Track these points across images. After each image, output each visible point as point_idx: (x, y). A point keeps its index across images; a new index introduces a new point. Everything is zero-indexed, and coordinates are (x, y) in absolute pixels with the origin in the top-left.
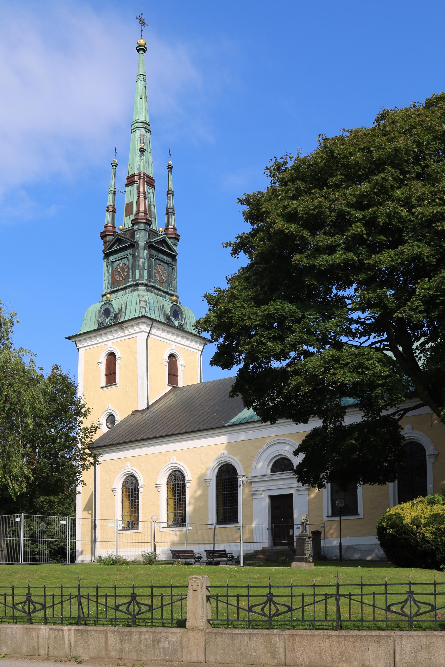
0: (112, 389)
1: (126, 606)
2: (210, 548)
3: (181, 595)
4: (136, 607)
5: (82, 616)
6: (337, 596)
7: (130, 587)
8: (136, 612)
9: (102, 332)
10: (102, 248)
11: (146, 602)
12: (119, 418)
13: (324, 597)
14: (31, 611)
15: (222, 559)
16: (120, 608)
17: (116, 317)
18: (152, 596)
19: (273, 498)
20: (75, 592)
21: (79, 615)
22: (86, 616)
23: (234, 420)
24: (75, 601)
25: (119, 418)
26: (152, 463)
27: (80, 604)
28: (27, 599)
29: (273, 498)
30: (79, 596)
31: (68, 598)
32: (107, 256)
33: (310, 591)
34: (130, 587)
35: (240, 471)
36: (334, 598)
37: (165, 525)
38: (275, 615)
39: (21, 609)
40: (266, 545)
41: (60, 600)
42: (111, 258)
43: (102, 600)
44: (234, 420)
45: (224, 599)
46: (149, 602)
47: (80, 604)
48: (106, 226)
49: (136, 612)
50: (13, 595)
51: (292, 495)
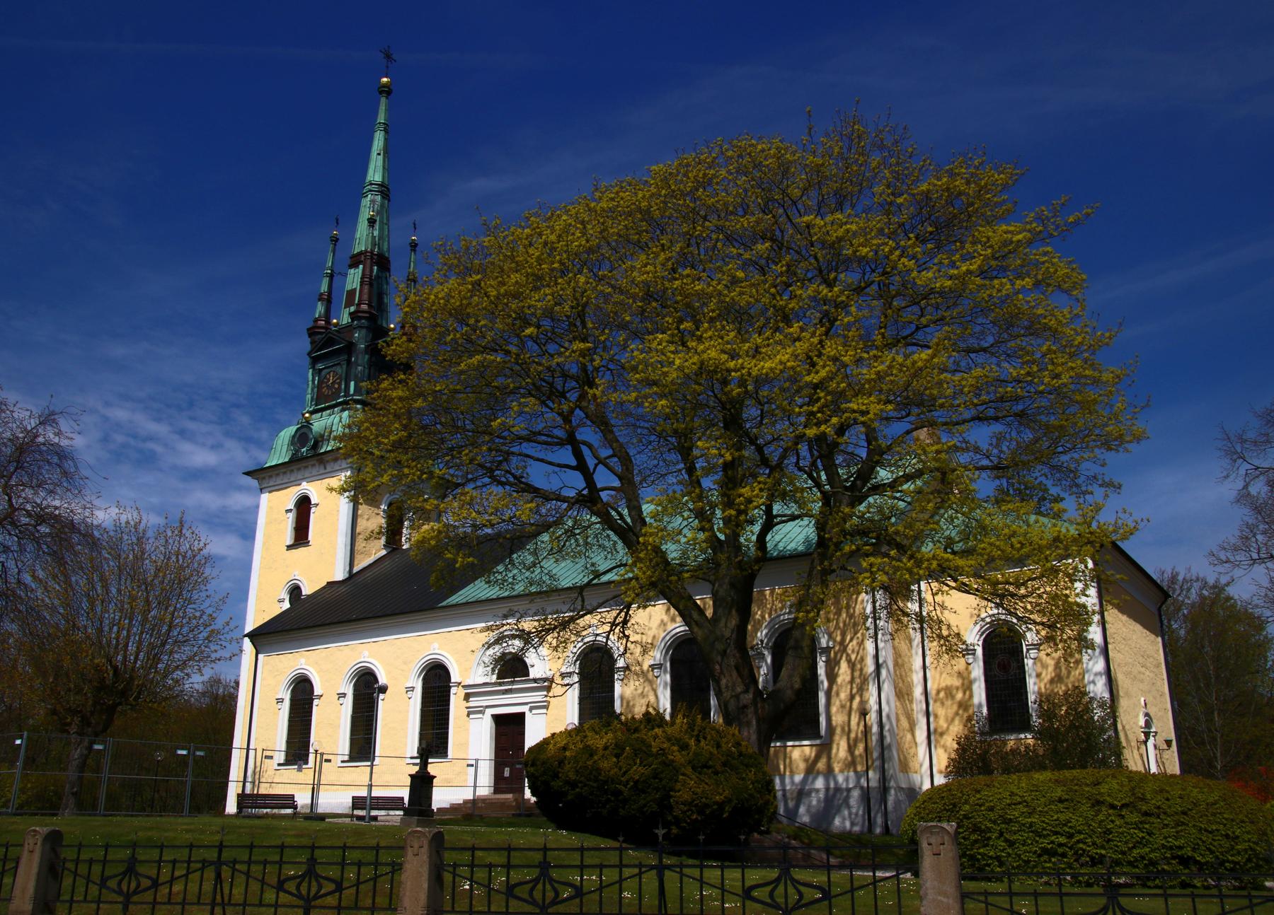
0: (302, 551)
1: (769, 888)
2: (363, 793)
3: (393, 864)
4: (791, 890)
5: (219, 897)
6: (219, 863)
7: (539, 850)
8: (312, 894)
9: (294, 467)
10: (308, 347)
11: (149, 874)
12: (307, 590)
13: (636, 871)
14: (547, 901)
15: (276, 811)
16: (517, 891)
17: (316, 445)
18: (343, 864)
19: (498, 719)
20: (212, 855)
21: (214, 898)
22: (226, 899)
23: (444, 603)
24: (210, 874)
25: (307, 590)
26: (330, 665)
27: (219, 876)
28: (541, 874)
29: (498, 719)
30: (219, 863)
31: (199, 865)
32: (315, 360)
33: (370, 857)
34: (539, 850)
35: (455, 677)
36: (654, 872)
37: (346, 758)
38: (798, 906)
39: (115, 887)
40: (485, 788)
41: (617, 878)
42: (320, 366)
43: (256, 869)
44: (444, 603)
45: (244, 868)
46: (153, 873)
47: (219, 876)
48: (316, 320)
49: (312, 894)
50: (508, 867)
51: (522, 715)
